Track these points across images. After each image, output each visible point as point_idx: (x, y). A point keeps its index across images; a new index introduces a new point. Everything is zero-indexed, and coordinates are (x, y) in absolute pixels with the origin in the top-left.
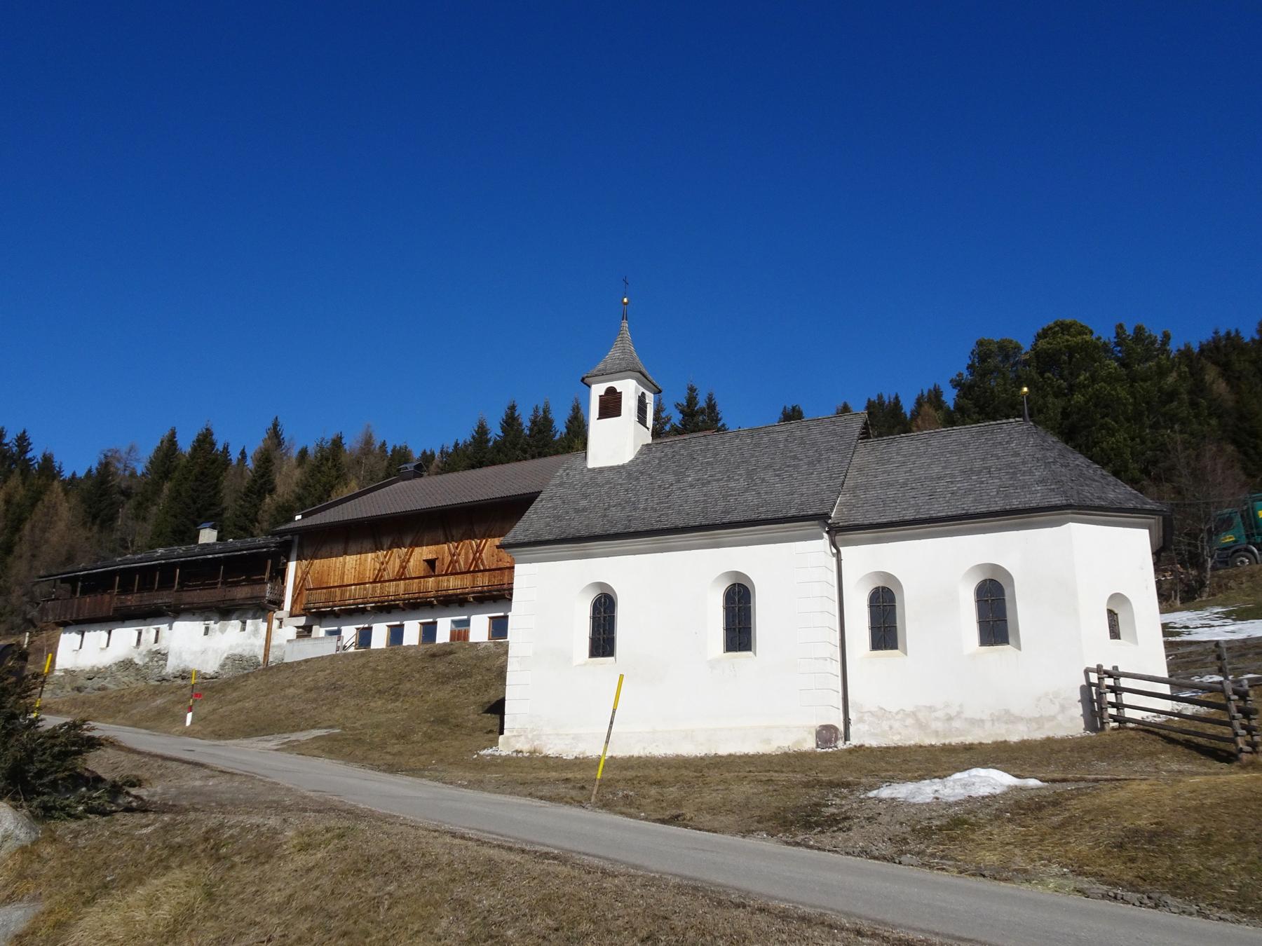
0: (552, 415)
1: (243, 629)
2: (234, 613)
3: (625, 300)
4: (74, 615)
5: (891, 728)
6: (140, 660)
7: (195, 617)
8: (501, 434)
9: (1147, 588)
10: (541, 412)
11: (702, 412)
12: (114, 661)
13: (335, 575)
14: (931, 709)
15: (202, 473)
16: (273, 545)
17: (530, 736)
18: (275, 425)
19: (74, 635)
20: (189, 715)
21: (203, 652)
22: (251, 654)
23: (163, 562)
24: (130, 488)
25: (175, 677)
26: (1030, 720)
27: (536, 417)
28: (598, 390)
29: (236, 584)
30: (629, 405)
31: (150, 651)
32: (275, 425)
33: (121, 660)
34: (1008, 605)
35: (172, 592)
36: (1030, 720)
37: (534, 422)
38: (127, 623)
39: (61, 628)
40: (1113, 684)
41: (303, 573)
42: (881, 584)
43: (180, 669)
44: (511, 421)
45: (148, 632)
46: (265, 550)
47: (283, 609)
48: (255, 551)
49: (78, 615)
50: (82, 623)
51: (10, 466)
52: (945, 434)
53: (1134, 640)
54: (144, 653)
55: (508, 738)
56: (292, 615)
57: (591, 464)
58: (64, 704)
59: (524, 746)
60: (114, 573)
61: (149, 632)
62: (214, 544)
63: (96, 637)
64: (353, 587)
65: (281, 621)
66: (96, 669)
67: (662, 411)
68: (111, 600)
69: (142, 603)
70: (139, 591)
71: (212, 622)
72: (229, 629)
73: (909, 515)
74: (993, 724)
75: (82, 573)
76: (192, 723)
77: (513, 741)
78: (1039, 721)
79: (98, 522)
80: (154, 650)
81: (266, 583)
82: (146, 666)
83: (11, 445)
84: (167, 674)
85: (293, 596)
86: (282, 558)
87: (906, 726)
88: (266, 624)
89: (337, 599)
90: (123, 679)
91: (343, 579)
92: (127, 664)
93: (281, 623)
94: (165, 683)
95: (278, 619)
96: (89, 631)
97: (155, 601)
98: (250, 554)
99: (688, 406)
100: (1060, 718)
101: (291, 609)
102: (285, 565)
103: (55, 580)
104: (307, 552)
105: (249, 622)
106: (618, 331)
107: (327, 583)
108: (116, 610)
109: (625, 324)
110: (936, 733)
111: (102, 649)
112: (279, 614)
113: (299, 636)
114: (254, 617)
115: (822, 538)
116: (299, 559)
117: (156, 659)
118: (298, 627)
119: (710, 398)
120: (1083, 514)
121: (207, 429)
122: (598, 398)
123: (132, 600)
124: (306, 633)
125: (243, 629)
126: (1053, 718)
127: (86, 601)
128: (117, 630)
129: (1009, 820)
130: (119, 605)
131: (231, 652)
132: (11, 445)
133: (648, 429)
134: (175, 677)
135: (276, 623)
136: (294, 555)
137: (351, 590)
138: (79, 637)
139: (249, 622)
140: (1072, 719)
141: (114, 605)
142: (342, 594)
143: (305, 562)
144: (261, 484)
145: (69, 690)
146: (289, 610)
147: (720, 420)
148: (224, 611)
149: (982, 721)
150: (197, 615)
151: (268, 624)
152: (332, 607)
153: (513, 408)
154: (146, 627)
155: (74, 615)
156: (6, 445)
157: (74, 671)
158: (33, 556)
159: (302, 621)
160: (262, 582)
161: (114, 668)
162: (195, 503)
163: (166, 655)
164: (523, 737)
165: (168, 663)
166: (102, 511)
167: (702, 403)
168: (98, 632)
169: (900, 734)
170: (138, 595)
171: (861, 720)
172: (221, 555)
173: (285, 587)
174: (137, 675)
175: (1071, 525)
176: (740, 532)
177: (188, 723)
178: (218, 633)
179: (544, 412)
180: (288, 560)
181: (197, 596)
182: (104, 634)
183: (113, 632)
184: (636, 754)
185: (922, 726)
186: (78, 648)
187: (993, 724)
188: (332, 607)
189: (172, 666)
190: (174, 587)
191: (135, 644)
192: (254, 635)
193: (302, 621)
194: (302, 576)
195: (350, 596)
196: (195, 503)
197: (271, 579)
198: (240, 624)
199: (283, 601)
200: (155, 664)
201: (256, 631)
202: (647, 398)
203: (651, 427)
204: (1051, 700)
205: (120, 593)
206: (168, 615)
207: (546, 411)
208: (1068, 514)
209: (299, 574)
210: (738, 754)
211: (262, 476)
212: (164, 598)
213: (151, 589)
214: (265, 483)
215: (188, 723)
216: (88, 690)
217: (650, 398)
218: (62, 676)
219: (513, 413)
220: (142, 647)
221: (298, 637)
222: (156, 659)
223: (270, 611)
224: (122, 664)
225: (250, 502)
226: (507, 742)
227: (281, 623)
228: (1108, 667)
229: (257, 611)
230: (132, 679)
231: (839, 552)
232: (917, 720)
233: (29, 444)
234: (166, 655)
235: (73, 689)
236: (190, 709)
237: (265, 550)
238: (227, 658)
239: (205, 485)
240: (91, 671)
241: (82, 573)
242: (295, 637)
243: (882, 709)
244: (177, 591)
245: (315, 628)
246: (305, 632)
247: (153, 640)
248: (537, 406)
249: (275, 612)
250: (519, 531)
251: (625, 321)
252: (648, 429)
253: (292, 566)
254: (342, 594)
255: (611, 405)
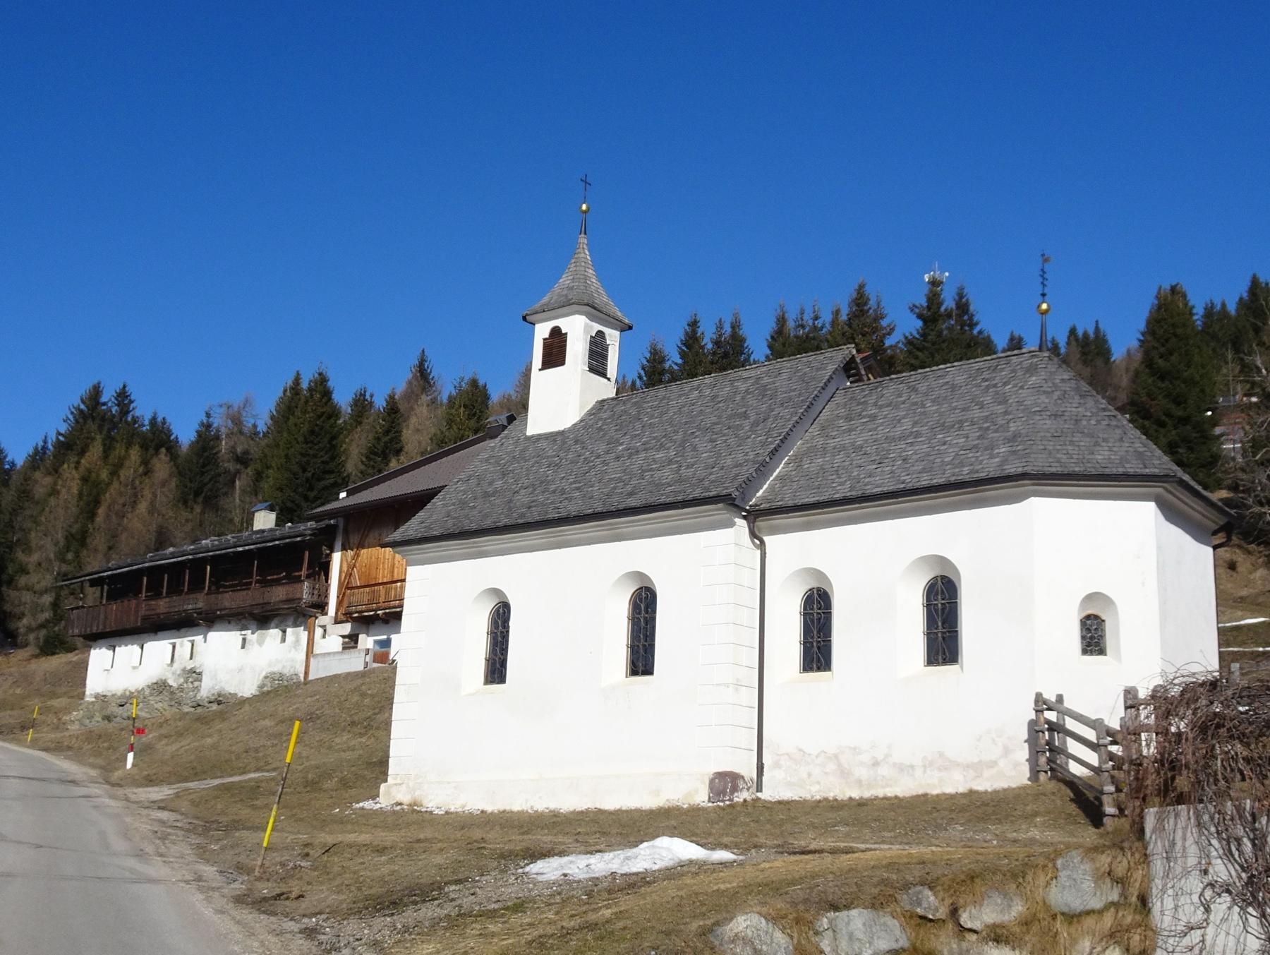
0: (745, 331)
1: (283, 640)
2: (273, 620)
3: (584, 207)
4: (101, 627)
5: (809, 775)
6: (175, 681)
7: (230, 626)
8: (680, 361)
9: (1143, 584)
10: (727, 329)
11: (949, 315)
12: (149, 682)
13: (384, 569)
14: (855, 750)
15: (312, 432)
16: (309, 532)
17: (411, 784)
18: (422, 362)
19: (104, 650)
20: (131, 756)
21: (240, 670)
22: (292, 671)
23: (190, 557)
24: (246, 452)
25: (210, 702)
26: (968, 766)
27: (720, 336)
28: (542, 331)
29: (277, 582)
30: (577, 350)
31: (184, 670)
32: (422, 362)
33: (155, 681)
34: (959, 609)
35: (203, 594)
36: (968, 766)
37: (717, 343)
38: (160, 634)
39: (255, 622)
40: (1055, 720)
41: (349, 566)
42: (815, 585)
43: (215, 692)
44: (691, 340)
45: (182, 645)
46: (299, 539)
47: (326, 614)
48: (288, 540)
49: (105, 627)
50: (113, 635)
51: (109, 431)
52: (939, 373)
53: (1118, 657)
54: (178, 672)
55: (389, 787)
56: (337, 621)
57: (529, 433)
58: (77, 738)
59: (405, 798)
60: (140, 572)
61: (183, 644)
62: (271, 530)
63: (127, 652)
64: (399, 584)
65: (324, 627)
66: (128, 693)
67: (882, 318)
68: (140, 606)
69: (173, 610)
70: (169, 594)
71: (250, 632)
72: (268, 640)
73: (842, 491)
74: (925, 772)
75: (105, 574)
76: (134, 765)
77: (394, 790)
78: (977, 768)
79: (200, 499)
80: (189, 668)
81: (303, 581)
82: (181, 688)
83: (110, 404)
84: (202, 700)
85: (338, 597)
86: (324, 548)
87: (826, 773)
88: (306, 633)
89: (382, 600)
90: (156, 706)
91: (393, 572)
92: (160, 687)
93: (325, 630)
94: (199, 710)
95: (321, 626)
96: (120, 646)
97: (185, 607)
98: (258, 549)
99: (929, 308)
100: (1002, 763)
101: (336, 613)
102: (329, 556)
103: (82, 582)
104: (354, 539)
105: (289, 630)
106: (573, 250)
107: (376, 578)
108: (145, 618)
109: (583, 240)
110: (859, 782)
111: (134, 668)
112: (322, 620)
113: (346, 647)
114: (296, 625)
115: (732, 525)
116: (344, 548)
117: (191, 680)
118: (343, 637)
119: (961, 296)
120: (827, 513)
121: (320, 374)
122: (542, 341)
123: (163, 606)
124: (352, 644)
125: (283, 640)
126: (993, 764)
127: (112, 609)
128: (149, 643)
129: (446, 929)
130: (147, 613)
131: (270, 670)
132: (110, 404)
133: (609, 379)
134: (210, 702)
135: (319, 631)
136: (338, 544)
137: (396, 588)
138: (111, 652)
139: (289, 630)
140: (1016, 765)
141: (142, 612)
142: (387, 593)
143: (350, 553)
144: (386, 443)
145: (100, 719)
146: (333, 615)
147: (977, 324)
148: (262, 618)
149: (912, 767)
150: (233, 623)
151: (309, 633)
152: (375, 610)
153: (694, 324)
154: (180, 640)
155: (101, 627)
156: (104, 404)
157: (105, 696)
158: (110, 548)
159: (347, 628)
160: (298, 580)
161: (147, 692)
162: (304, 470)
163: (200, 674)
164: (404, 786)
165: (203, 684)
166: (206, 484)
167: (949, 302)
168: (130, 647)
169: (818, 783)
170: (167, 600)
171: (777, 765)
172: (252, 547)
173: (329, 585)
174: (171, 700)
175: (1034, 500)
176: (638, 521)
177: (129, 765)
178: (256, 645)
179: (733, 327)
180: (332, 551)
181: (229, 600)
182: (136, 648)
183: (145, 645)
184: (516, 808)
185: (843, 773)
186: (109, 668)
187: (925, 772)
188: (375, 610)
189: (207, 688)
190: (204, 588)
191: (169, 662)
192: (295, 647)
193: (347, 628)
194: (348, 570)
195: (395, 596)
196: (304, 470)
197: (308, 577)
198: (280, 633)
199: (327, 604)
200: (191, 686)
201: (297, 641)
202: (607, 337)
203: (613, 380)
204: (994, 740)
205: (148, 598)
206: (198, 625)
207: (735, 326)
208: (1027, 485)
209: (345, 568)
210: (624, 808)
211: (387, 432)
212: (196, 603)
213: (180, 592)
214: (391, 440)
215: (129, 765)
216: (118, 719)
217: (613, 337)
218: (93, 702)
219: (694, 332)
220: (176, 665)
221: (344, 648)
222: (191, 680)
223: (311, 616)
224: (155, 687)
225: (373, 467)
226: (388, 793)
227: (325, 630)
228: (1051, 696)
229: (298, 617)
230: (165, 705)
231: (762, 542)
232: (840, 765)
233: (131, 402)
234: (200, 674)
235: (103, 719)
236: (131, 748)
237: (299, 539)
238: (266, 677)
239: (317, 447)
240: (123, 696)
241: (105, 574)
242: (340, 649)
243: (800, 750)
244: (207, 594)
245: (362, 637)
246: (351, 641)
247: (189, 656)
248: (720, 320)
249: (317, 618)
250: (411, 528)
251: (583, 235)
252: (609, 379)
253: (337, 557)
254: (387, 593)
255: (555, 353)
